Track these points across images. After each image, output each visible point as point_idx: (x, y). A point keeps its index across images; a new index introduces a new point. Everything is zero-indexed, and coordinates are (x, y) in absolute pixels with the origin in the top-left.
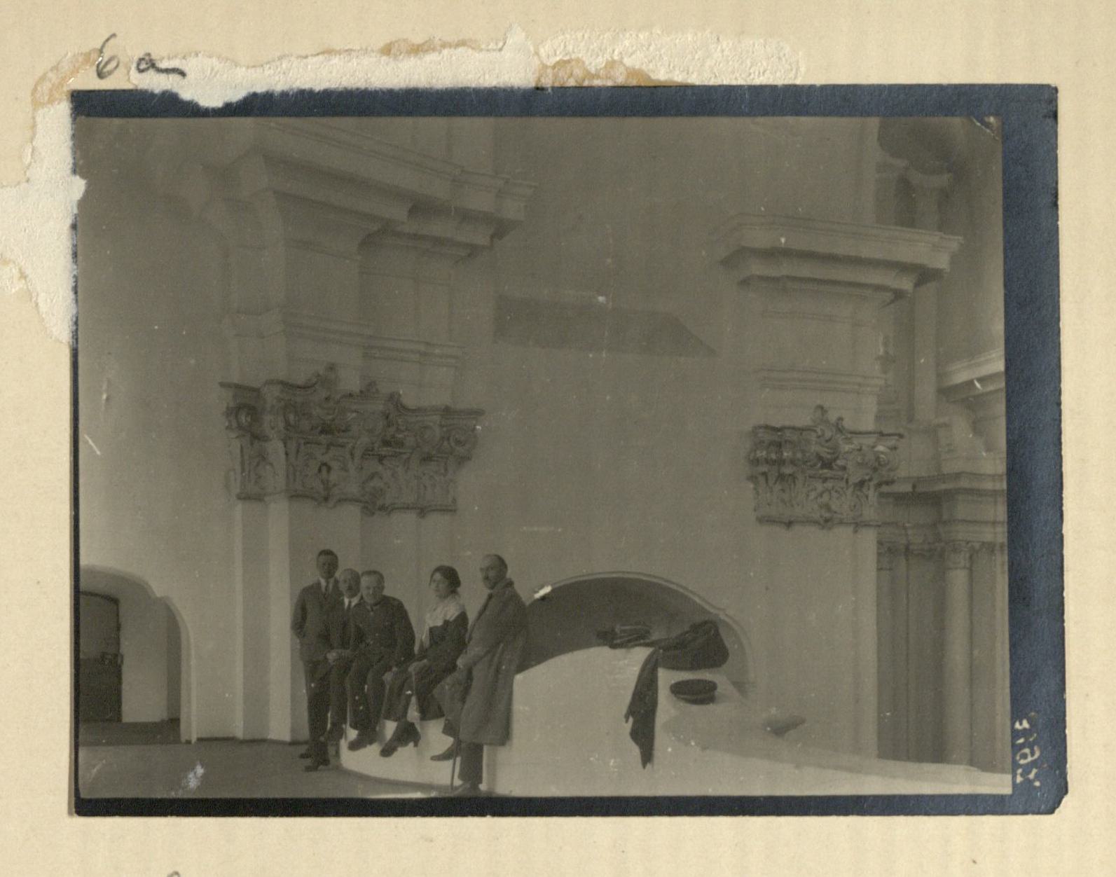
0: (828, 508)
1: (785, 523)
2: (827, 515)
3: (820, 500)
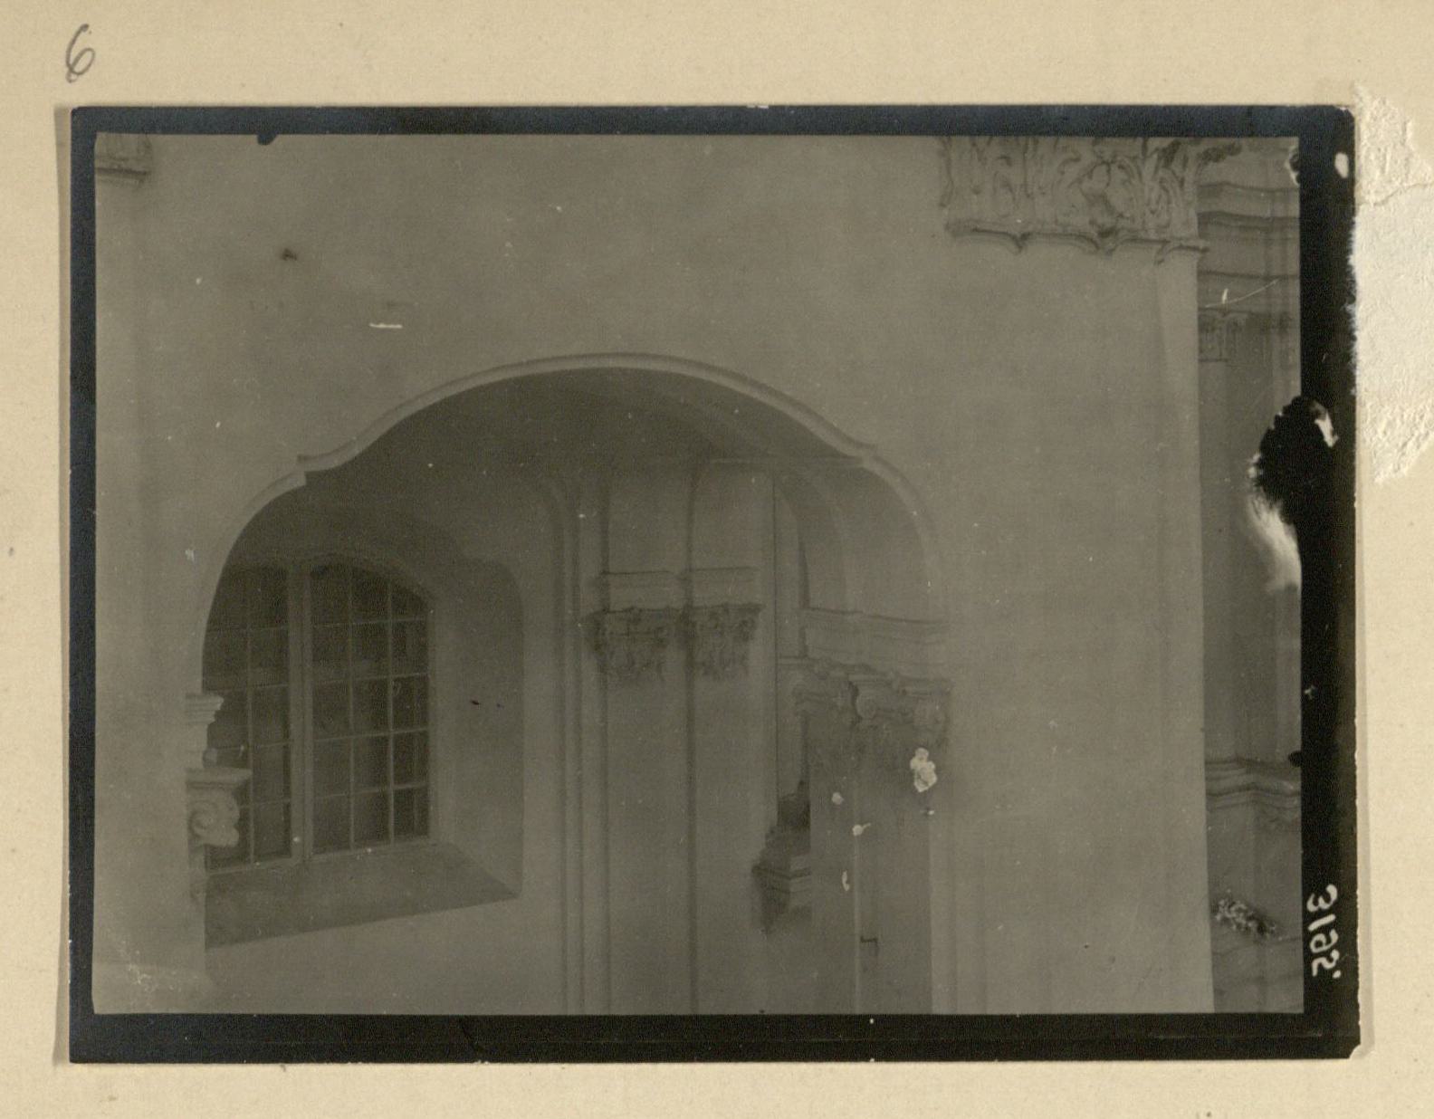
0: (1101, 200)
1: (1014, 238)
2: (1107, 221)
3: (1086, 185)
